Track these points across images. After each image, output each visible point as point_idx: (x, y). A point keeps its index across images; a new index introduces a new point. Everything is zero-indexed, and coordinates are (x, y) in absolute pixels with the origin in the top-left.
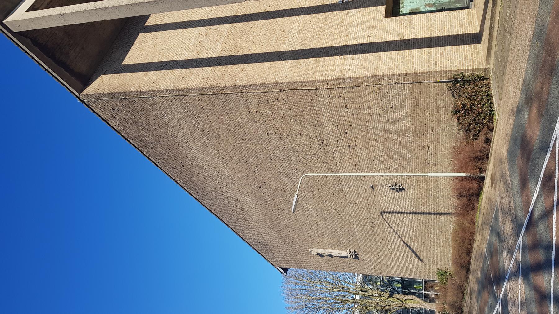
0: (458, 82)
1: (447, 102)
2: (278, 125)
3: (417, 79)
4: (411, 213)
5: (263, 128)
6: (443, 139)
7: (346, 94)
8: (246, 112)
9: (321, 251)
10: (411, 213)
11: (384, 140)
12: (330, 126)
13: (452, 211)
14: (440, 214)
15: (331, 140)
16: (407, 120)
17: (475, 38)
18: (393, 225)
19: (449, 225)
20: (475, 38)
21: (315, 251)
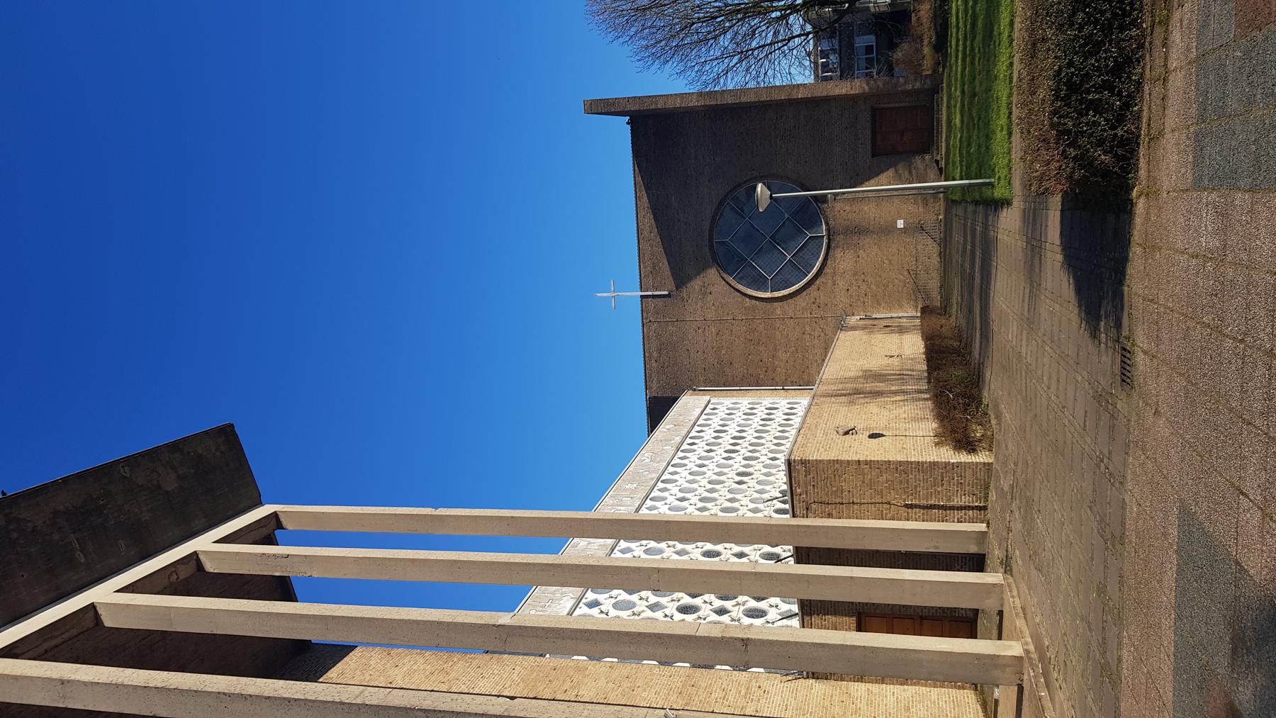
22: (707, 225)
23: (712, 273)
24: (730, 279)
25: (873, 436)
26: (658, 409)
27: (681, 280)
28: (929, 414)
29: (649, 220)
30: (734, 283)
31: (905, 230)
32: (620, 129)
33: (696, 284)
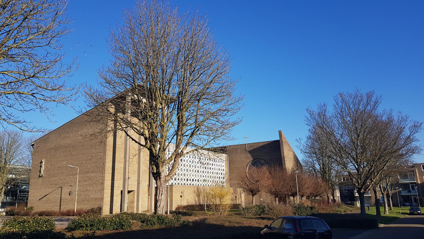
0: (100, 209)
1: (96, 207)
2: (94, 160)
3: (102, 199)
4: (61, 197)
5: (94, 155)
6: (85, 206)
7: (101, 181)
8: (99, 151)
9: (43, 163)
10: (61, 197)
11: (87, 190)
12: (92, 175)
13: (61, 210)
14: (60, 206)
15: (88, 175)
16: (92, 196)
17: (111, 212)
18: (55, 191)
19: (56, 209)
20: (111, 212)
21: (43, 161)
22: (260, 158)
23: (252, 159)
24: (250, 163)
25: (181, 196)
26: (223, 150)
27: (250, 152)
28: (190, 204)
29: (261, 145)
30: (249, 165)
31: (260, 200)
32: (278, 138)
33: (249, 156)
